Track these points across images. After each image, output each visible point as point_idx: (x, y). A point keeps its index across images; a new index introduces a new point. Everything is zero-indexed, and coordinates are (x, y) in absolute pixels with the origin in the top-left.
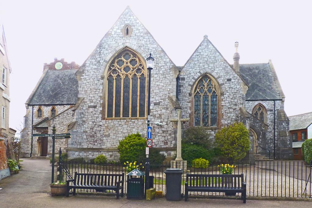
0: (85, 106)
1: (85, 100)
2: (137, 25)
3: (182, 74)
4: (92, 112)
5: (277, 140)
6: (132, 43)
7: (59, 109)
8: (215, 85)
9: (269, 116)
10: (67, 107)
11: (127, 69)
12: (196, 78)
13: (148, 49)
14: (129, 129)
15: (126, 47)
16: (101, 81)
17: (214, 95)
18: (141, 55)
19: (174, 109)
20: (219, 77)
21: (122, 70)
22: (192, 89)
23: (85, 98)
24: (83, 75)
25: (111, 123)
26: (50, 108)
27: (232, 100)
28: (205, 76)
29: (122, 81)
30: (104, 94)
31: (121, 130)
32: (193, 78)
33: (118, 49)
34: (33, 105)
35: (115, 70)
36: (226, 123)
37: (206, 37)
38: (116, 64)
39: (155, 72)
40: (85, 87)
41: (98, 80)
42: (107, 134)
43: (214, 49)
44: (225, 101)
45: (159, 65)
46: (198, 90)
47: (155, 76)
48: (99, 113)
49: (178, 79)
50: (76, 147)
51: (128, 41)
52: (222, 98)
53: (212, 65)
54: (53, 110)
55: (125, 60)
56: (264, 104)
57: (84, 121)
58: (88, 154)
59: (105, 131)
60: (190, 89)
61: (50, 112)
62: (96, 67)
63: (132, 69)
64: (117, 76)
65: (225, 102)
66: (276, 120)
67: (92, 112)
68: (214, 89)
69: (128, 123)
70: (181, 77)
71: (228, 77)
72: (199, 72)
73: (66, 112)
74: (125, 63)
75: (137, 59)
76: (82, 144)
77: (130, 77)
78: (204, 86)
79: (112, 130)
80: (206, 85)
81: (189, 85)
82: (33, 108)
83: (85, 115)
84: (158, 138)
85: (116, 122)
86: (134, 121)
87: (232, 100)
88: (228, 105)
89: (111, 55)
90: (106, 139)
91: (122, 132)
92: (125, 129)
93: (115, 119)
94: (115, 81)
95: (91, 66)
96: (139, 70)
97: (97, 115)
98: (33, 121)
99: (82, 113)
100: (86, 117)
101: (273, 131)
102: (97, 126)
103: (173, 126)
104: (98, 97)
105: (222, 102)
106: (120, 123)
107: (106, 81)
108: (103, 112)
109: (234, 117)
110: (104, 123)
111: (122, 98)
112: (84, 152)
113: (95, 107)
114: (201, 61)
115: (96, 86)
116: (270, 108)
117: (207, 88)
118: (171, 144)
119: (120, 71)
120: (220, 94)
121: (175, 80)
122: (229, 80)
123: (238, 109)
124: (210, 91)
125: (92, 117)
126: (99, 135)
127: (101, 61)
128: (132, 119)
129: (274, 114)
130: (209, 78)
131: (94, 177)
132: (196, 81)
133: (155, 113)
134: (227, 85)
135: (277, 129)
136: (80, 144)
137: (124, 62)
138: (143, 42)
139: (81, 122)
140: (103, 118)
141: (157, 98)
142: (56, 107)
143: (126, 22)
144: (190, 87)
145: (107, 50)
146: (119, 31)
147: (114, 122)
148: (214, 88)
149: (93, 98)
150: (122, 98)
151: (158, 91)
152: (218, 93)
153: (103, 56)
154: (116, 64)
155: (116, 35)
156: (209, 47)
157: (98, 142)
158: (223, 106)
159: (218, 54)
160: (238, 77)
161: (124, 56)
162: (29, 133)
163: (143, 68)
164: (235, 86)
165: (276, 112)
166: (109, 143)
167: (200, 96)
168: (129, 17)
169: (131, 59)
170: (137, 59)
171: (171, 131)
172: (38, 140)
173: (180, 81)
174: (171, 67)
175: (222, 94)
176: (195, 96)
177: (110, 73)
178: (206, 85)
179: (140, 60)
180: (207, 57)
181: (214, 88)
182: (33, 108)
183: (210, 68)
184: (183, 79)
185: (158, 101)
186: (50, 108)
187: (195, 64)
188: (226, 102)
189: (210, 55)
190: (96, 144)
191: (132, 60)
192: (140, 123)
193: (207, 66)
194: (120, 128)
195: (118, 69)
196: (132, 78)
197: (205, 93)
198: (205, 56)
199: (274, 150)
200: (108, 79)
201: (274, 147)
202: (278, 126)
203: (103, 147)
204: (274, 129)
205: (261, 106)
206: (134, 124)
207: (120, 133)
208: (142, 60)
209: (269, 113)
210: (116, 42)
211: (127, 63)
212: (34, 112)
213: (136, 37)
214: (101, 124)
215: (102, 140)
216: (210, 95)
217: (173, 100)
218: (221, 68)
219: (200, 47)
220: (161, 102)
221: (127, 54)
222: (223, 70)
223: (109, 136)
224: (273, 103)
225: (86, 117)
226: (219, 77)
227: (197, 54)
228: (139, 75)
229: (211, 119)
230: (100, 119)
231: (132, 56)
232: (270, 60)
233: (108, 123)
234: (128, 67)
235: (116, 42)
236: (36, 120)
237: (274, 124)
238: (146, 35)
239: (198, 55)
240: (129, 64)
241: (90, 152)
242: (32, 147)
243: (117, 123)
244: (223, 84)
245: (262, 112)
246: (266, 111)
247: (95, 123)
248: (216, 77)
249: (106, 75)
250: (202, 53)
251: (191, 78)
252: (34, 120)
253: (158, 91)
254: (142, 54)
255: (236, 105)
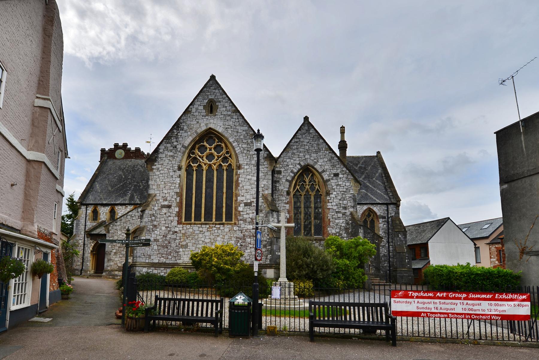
0: (157, 205)
1: (157, 198)
2: (224, 101)
3: (278, 166)
4: (165, 214)
5: (393, 258)
6: (217, 124)
7: (120, 211)
8: (319, 182)
9: (381, 225)
10: (130, 208)
11: (210, 157)
12: (295, 171)
13: (237, 132)
14: (212, 237)
15: (210, 128)
16: (178, 173)
17: (318, 196)
18: (227, 139)
19: (270, 212)
20: (324, 171)
21: (204, 158)
22: (290, 186)
23: (158, 195)
24: (155, 163)
25: (189, 229)
26: (108, 208)
27: (341, 202)
28: (307, 170)
29: (204, 172)
30: (182, 189)
31: (203, 239)
32: (292, 172)
33: (199, 131)
34: (87, 205)
35: (195, 158)
36: (334, 231)
37: (306, 119)
38: (197, 151)
39: (246, 163)
40: (158, 180)
41: (175, 171)
42: (184, 243)
43: (316, 134)
44: (331, 202)
45: (251, 153)
46: (298, 187)
47: (246, 167)
48: (174, 215)
49: (273, 172)
50: (143, 261)
51: (212, 121)
52: (328, 198)
53: (315, 155)
54: (113, 212)
55: (208, 146)
56: (375, 209)
57: (155, 226)
58: (159, 271)
59: (182, 240)
60: (288, 186)
61: (108, 214)
62: (171, 154)
63: (216, 157)
64: (198, 166)
65: (333, 203)
66: (390, 231)
67: (165, 214)
68: (317, 187)
69: (211, 230)
70: (277, 169)
71: (335, 171)
72: (299, 164)
73: (130, 213)
74: (208, 149)
75: (223, 145)
76: (152, 257)
77: (215, 167)
78: (305, 182)
79: (191, 239)
80: (307, 180)
81: (287, 180)
82: (87, 208)
83: (156, 217)
84: (249, 251)
85: (196, 228)
86: (218, 226)
87: (341, 202)
88: (335, 208)
89: (190, 139)
90: (183, 251)
91: (203, 242)
92: (207, 237)
93: (195, 224)
94: (195, 172)
95: (166, 152)
96: (225, 159)
97: (172, 218)
98: (85, 226)
99: (153, 215)
100: (158, 220)
101: (387, 245)
102: (171, 233)
103: (268, 235)
104: (173, 194)
105: (328, 204)
106: (201, 229)
107: (183, 173)
108: (179, 214)
109: (343, 225)
110: (181, 229)
111: (204, 195)
112: (154, 268)
113: (169, 207)
114: (301, 150)
115: (171, 179)
116: (382, 214)
117: (309, 185)
118: (266, 259)
119: (201, 160)
120: (324, 194)
121: (270, 173)
122: (336, 175)
123: (348, 213)
124: (312, 188)
125: (165, 220)
126: (173, 245)
127: (179, 147)
128: (216, 224)
129: (388, 222)
130: (311, 172)
131: (172, 303)
132: (295, 176)
133: (245, 216)
134: (333, 182)
135: (392, 242)
136: (150, 256)
137: (206, 148)
138: (231, 123)
139: (151, 227)
140: (179, 223)
141: (248, 197)
142: (116, 208)
143: (210, 97)
144: (288, 183)
145: (186, 131)
146: (202, 108)
147: (194, 228)
148: (317, 186)
149: (167, 195)
150: (204, 195)
151: (249, 187)
152: (323, 192)
153: (180, 139)
154: (197, 151)
155: (197, 114)
156: (311, 131)
157: (172, 254)
158: (329, 209)
159: (321, 141)
160: (347, 171)
161: (207, 141)
162: (80, 241)
163: (230, 156)
164: (344, 183)
165: (390, 220)
166: (186, 256)
167: (301, 195)
168: (214, 91)
169: (215, 144)
170: (223, 145)
171: (266, 241)
172: (92, 251)
173: (276, 175)
174: (265, 155)
175: (328, 194)
176: (294, 195)
177: (189, 162)
178: (307, 180)
179: (226, 146)
180: (308, 144)
181: (317, 186)
182: (87, 208)
183: (312, 158)
184: (279, 172)
185: (249, 201)
186: (108, 208)
187: (293, 153)
188: (333, 204)
189: (312, 143)
190: (170, 257)
191: (217, 145)
192: (227, 230)
193: (308, 157)
194: (200, 236)
195: (200, 156)
196: (217, 170)
197: (306, 192)
198: (306, 143)
199: (389, 270)
200: (186, 170)
201: (390, 267)
202: (392, 239)
203: (178, 261)
204: (388, 242)
205: (370, 211)
206: (220, 231)
207: (200, 242)
208: (229, 145)
209: (381, 220)
210: (198, 122)
211: (210, 149)
212: (88, 214)
213: (222, 116)
214: (177, 229)
215: (178, 252)
216: (313, 194)
217: (268, 200)
218: (326, 160)
219: (299, 132)
220: (253, 202)
221: (211, 137)
222: (329, 162)
223: (186, 246)
224: (386, 208)
225: (158, 220)
226: (324, 171)
227: (296, 140)
228: (225, 165)
229: (315, 226)
230: (175, 223)
231: (217, 140)
232: (378, 153)
233: (185, 228)
234: (212, 154)
235: (198, 122)
236: (90, 224)
237: (388, 235)
238: (235, 114)
239: (297, 142)
240: (213, 151)
241: (161, 269)
242: (83, 262)
243: (197, 228)
244: (329, 180)
245: (372, 219)
246: (378, 217)
247: (168, 229)
248: (320, 171)
249: (184, 165)
250: (302, 140)
251: (289, 171)
252: (87, 224)
253: (249, 187)
254: (230, 139)
255: (345, 208)
